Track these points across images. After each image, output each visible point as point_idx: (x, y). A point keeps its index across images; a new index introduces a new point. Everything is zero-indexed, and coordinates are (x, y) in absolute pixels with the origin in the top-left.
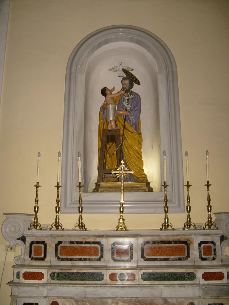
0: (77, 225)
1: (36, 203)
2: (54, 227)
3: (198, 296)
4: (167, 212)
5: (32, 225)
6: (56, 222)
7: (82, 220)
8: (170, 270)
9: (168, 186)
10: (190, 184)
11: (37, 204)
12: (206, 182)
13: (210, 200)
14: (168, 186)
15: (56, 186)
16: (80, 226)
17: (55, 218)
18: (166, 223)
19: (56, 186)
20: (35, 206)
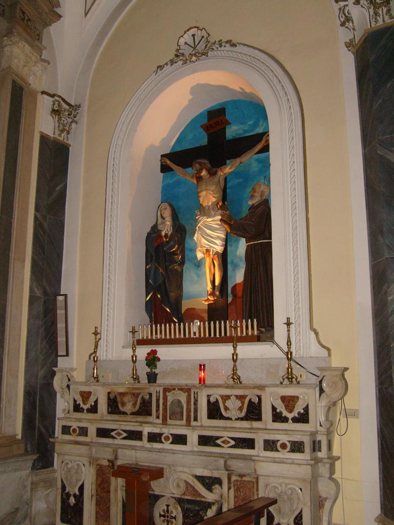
0: (230, 377)
1: (288, 347)
2: (286, 380)
3: (139, 451)
4: (135, 362)
5: (285, 377)
6: (288, 373)
7: (136, 371)
8: (175, 430)
9: (292, 323)
10: (291, 322)
11: (290, 348)
12: (286, 319)
13: (290, 345)
14: (292, 323)
15: (285, 323)
16: (134, 378)
17: (232, 368)
18: (288, 374)
19: (285, 323)
20: (233, 352)
